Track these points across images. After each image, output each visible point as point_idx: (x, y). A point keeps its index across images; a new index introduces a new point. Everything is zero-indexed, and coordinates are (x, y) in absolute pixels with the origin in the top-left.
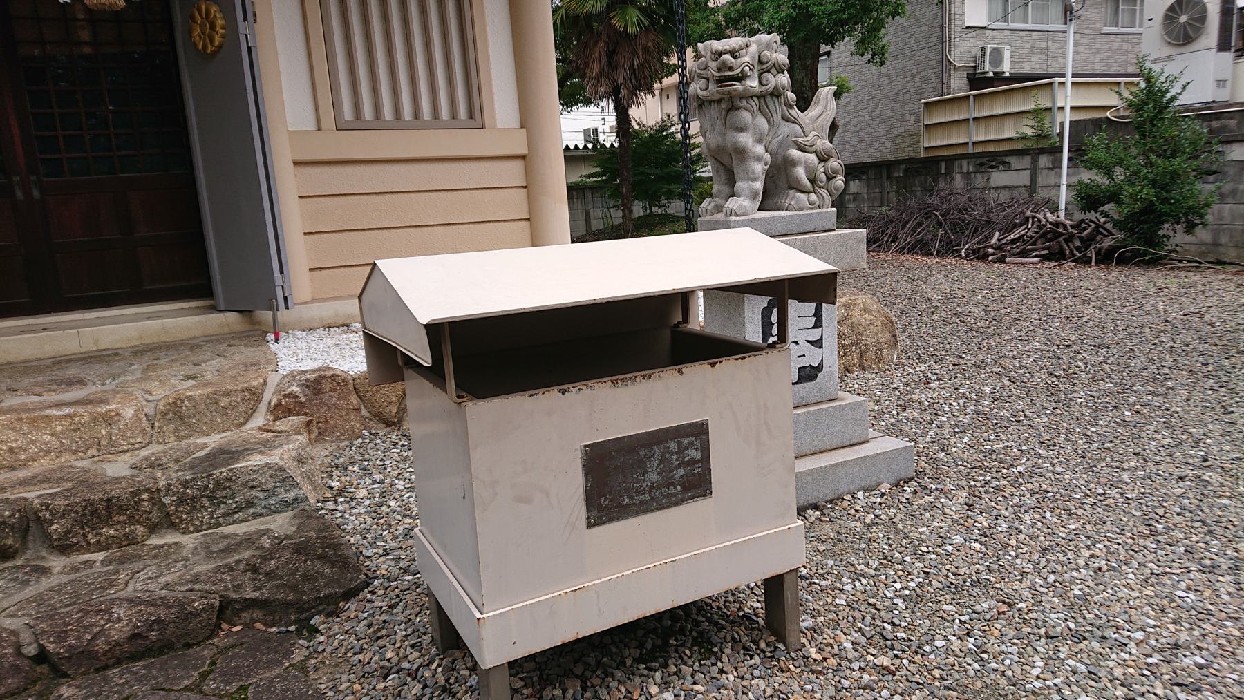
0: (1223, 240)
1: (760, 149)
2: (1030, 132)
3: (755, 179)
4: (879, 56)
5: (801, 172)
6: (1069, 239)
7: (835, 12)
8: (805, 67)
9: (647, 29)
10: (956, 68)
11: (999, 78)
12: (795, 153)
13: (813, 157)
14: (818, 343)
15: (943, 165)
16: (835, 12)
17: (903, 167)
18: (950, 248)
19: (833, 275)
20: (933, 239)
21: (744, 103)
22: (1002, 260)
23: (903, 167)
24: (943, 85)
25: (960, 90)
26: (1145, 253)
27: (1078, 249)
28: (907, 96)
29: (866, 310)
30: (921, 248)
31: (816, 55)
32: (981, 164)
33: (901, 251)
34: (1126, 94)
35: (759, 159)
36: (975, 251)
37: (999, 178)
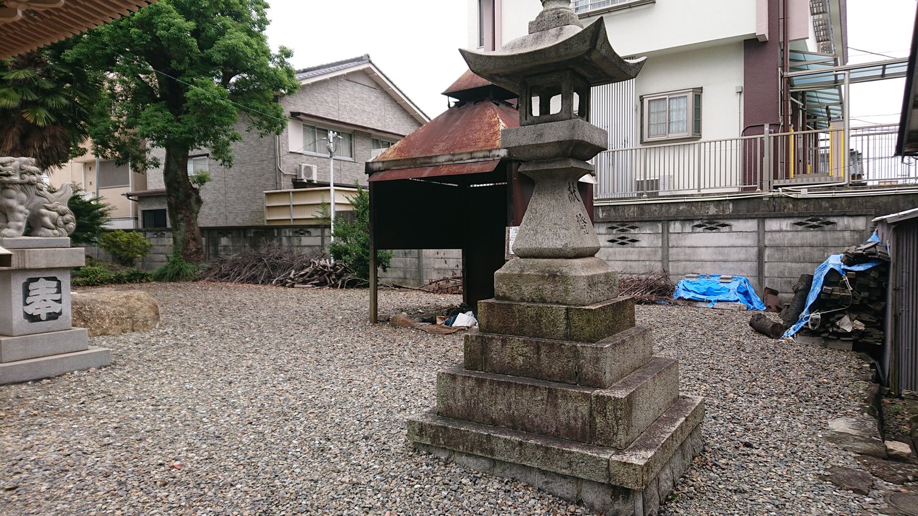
0: (408, 276)
1: (22, 208)
2: (320, 216)
3: (19, 221)
4: (228, 162)
5: (47, 220)
6: (330, 275)
7: (185, 133)
8: (178, 162)
9: (54, 124)
10: (284, 175)
11: (310, 183)
12: (44, 211)
13: (55, 214)
14: (59, 301)
15: (276, 231)
16: (185, 133)
17: (253, 231)
18: (267, 281)
19: (11, 255)
20: (260, 275)
21: (11, 186)
22: (292, 286)
23: (253, 231)
24: (277, 184)
25: (288, 188)
26: (362, 281)
27: (334, 280)
28: (257, 188)
29: (138, 300)
30: (253, 280)
31: (186, 158)
32: (296, 232)
33: (242, 282)
34: (351, 199)
35: (21, 212)
36: (282, 281)
37: (306, 240)
